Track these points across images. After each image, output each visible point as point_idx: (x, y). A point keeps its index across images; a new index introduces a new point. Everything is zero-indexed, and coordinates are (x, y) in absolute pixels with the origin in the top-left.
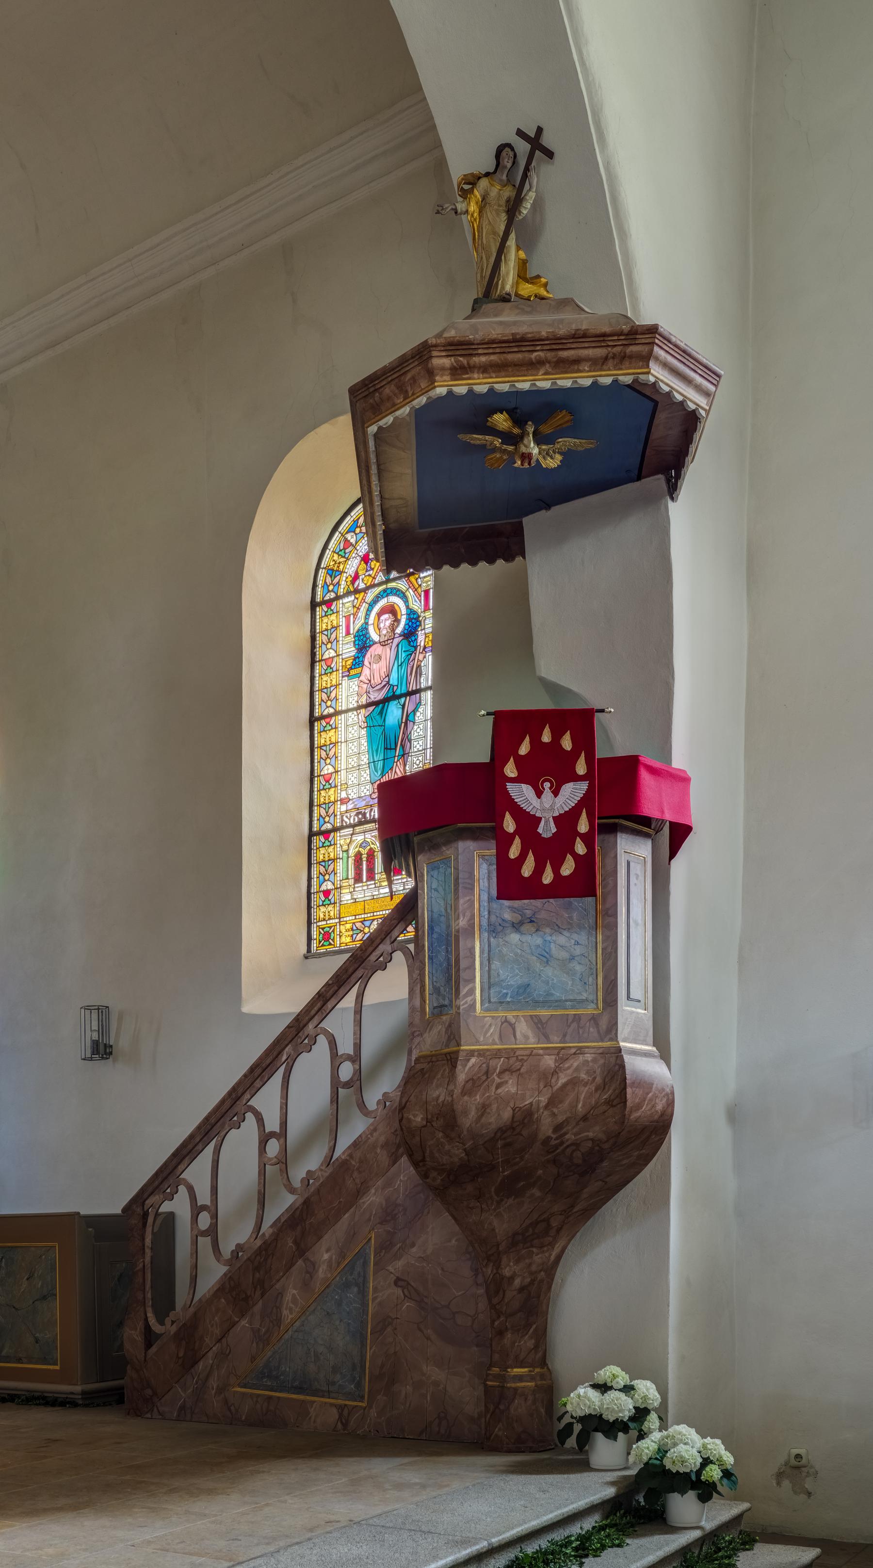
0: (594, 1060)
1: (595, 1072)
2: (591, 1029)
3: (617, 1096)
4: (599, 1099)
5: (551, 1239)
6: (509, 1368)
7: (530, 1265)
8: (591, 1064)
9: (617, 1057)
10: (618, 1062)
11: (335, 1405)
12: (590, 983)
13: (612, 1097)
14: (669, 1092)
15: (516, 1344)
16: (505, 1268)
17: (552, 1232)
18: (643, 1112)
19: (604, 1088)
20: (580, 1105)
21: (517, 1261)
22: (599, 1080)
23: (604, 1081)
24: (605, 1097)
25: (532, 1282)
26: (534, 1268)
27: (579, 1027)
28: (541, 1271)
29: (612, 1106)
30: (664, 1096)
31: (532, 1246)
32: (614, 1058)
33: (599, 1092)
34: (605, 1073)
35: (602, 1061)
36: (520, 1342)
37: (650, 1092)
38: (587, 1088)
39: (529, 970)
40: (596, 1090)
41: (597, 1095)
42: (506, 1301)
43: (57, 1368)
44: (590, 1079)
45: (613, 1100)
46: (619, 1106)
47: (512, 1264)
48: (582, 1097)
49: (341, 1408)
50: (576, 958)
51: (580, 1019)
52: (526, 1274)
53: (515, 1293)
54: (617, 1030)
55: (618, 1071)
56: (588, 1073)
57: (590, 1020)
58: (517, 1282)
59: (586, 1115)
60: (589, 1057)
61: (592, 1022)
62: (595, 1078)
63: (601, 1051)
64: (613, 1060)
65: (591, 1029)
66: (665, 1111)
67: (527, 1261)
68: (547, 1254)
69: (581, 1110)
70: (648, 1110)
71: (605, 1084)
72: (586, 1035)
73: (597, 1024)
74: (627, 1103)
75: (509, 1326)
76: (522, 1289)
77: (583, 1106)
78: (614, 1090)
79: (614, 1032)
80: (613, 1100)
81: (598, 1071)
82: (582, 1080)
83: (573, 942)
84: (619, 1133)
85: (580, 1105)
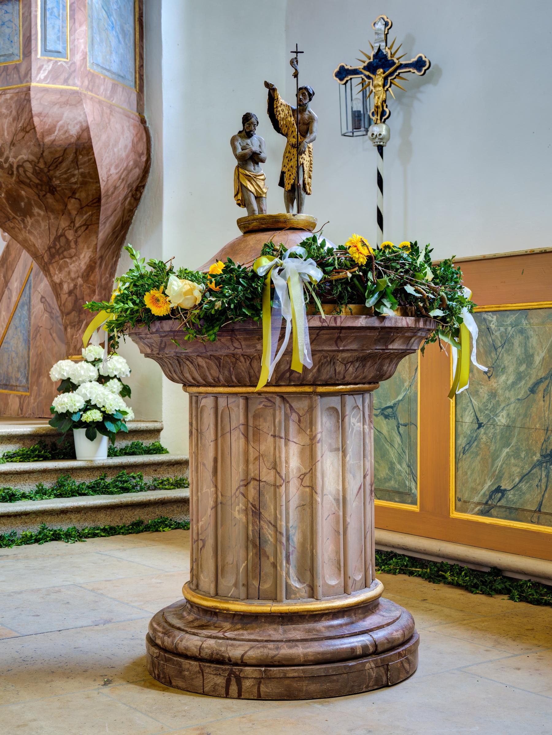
0: (11, 98)
1: (11, 107)
2: (15, 76)
3: (28, 124)
4: (16, 127)
5: (74, 250)
6: (70, 355)
7: (69, 273)
8: (9, 101)
9: (26, 94)
10: (27, 98)
11: (17, 396)
12: (15, 41)
13: (25, 125)
14: (83, 120)
15: (74, 337)
16: (54, 276)
17: (72, 244)
18: (56, 136)
19: (18, 119)
20: (6, 134)
21: (60, 270)
22: (14, 113)
23: (18, 113)
24: (20, 125)
25: (75, 286)
26: (73, 275)
27: (7, 75)
28: (78, 277)
29: (27, 132)
30: (77, 124)
31: (64, 257)
32: (24, 95)
33: (15, 122)
34: (18, 107)
35: (16, 98)
36: (76, 335)
37: (60, 120)
38: (7, 120)
39: (11, 41)
40: (14, 120)
41: (15, 124)
42: (63, 302)
43: (415, 508)
44: (9, 112)
45: (26, 128)
46: (31, 132)
47: (57, 272)
48: (5, 126)
49: (20, 397)
50: (6, 24)
51: (7, 69)
52: (69, 281)
53: (67, 296)
54: (31, 74)
55: (26, 104)
56: (7, 108)
57: (14, 69)
58: (65, 286)
59: (12, 141)
60: (8, 96)
61: (15, 70)
62: (11, 112)
63: (17, 91)
64: (23, 96)
65: (15, 76)
66: (80, 136)
67: (66, 269)
68: (77, 263)
69: (7, 137)
70: (62, 135)
71: (18, 115)
72: (11, 80)
73: (18, 71)
74: (36, 129)
75: (68, 323)
76: (70, 293)
77: (8, 134)
78: (25, 120)
79: (29, 76)
80: (26, 128)
81: (13, 106)
82: (4, 114)
83: (3, 11)
84: (42, 154)
85: (6, 134)
